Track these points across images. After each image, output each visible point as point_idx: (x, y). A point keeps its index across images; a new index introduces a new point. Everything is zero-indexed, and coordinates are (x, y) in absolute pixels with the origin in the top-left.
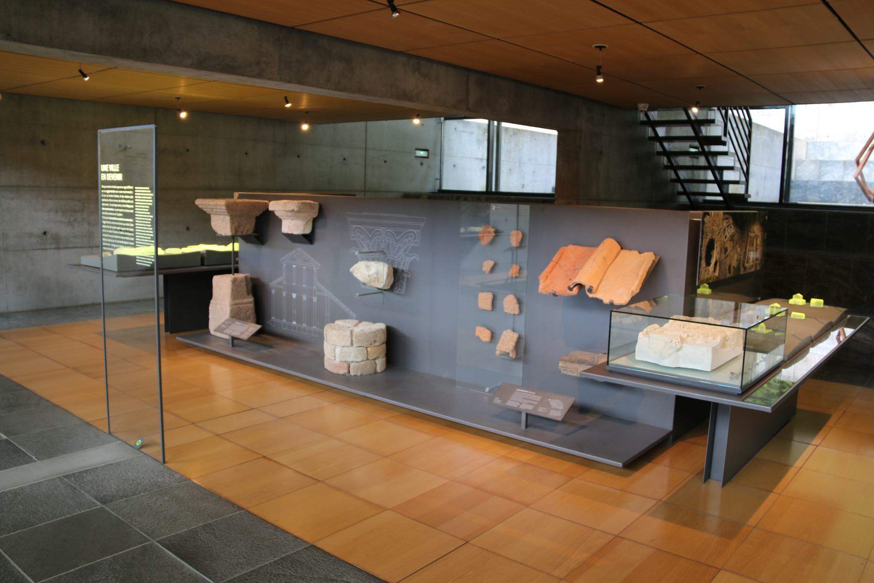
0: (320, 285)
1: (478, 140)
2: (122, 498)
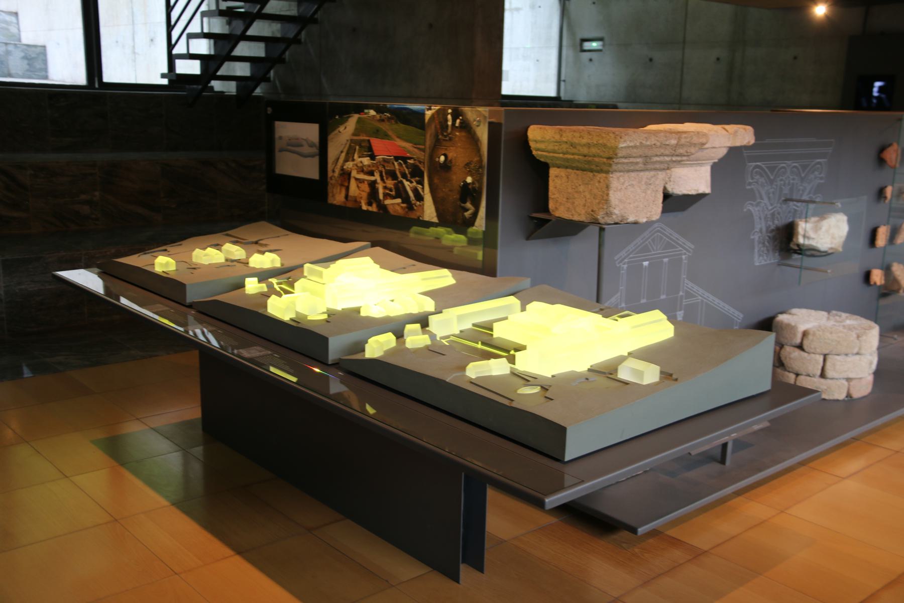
0: (690, 285)
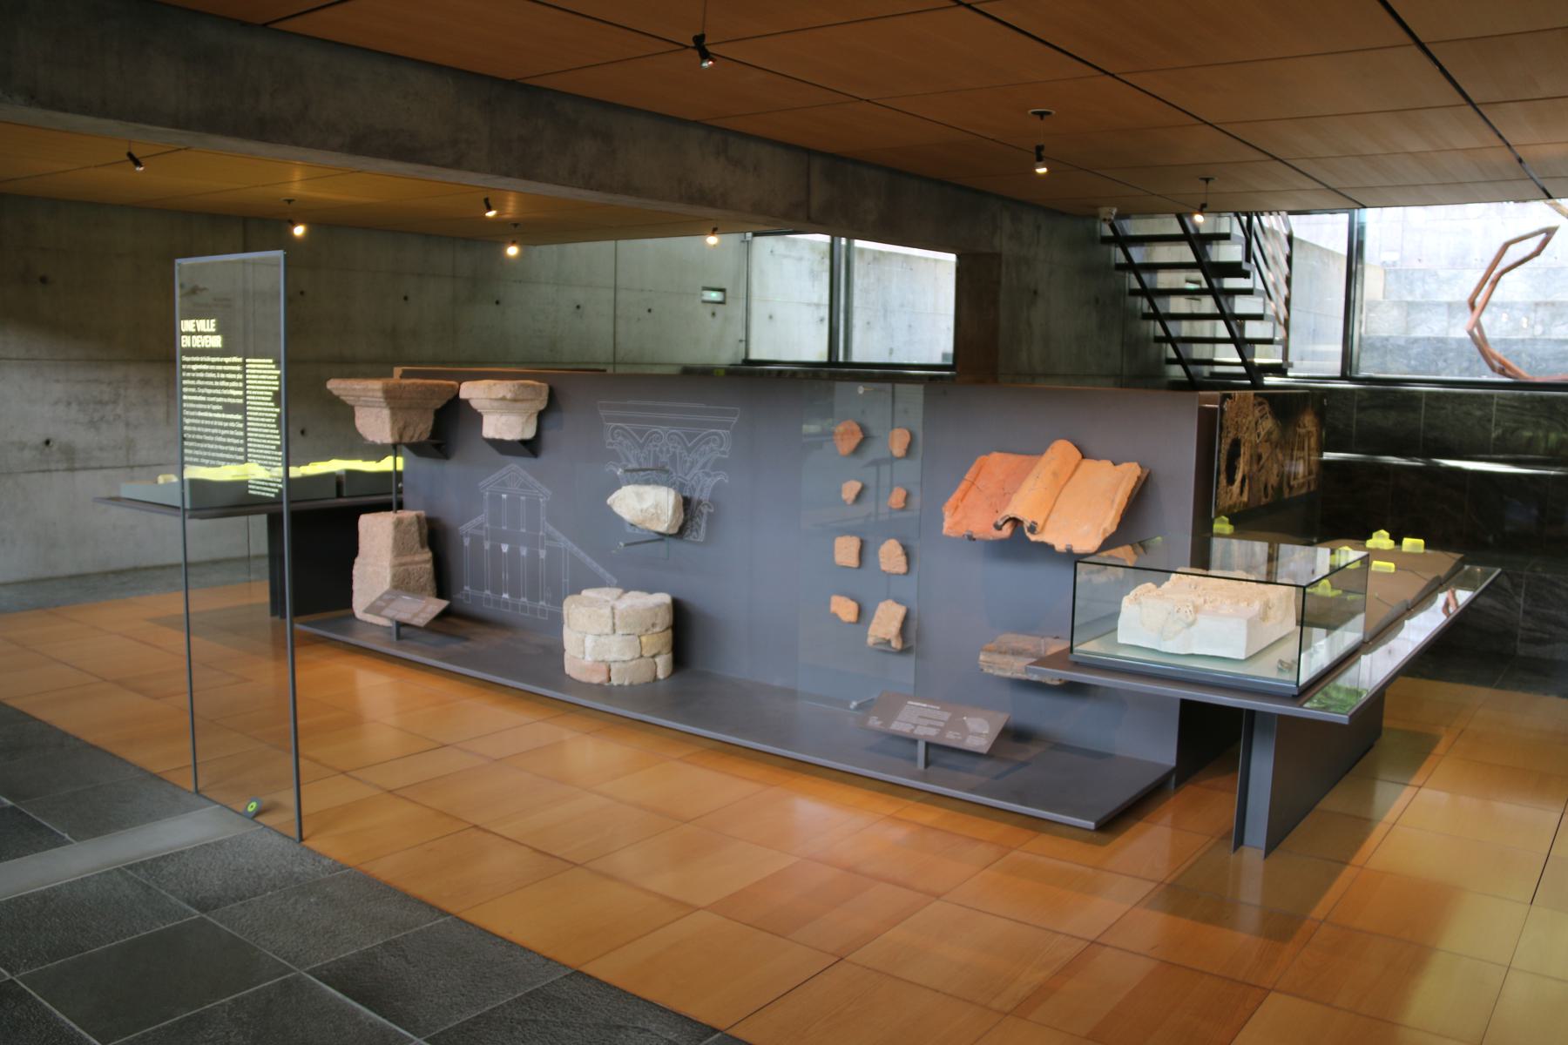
0: (551, 528)
1: (812, 271)
2: (235, 902)
